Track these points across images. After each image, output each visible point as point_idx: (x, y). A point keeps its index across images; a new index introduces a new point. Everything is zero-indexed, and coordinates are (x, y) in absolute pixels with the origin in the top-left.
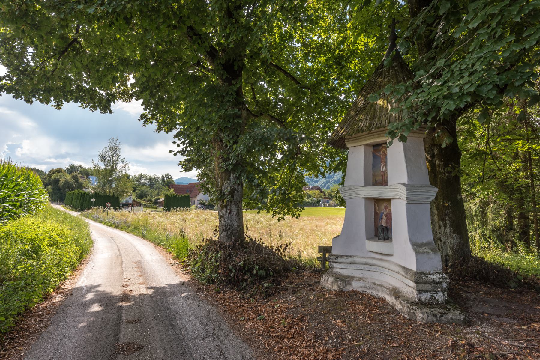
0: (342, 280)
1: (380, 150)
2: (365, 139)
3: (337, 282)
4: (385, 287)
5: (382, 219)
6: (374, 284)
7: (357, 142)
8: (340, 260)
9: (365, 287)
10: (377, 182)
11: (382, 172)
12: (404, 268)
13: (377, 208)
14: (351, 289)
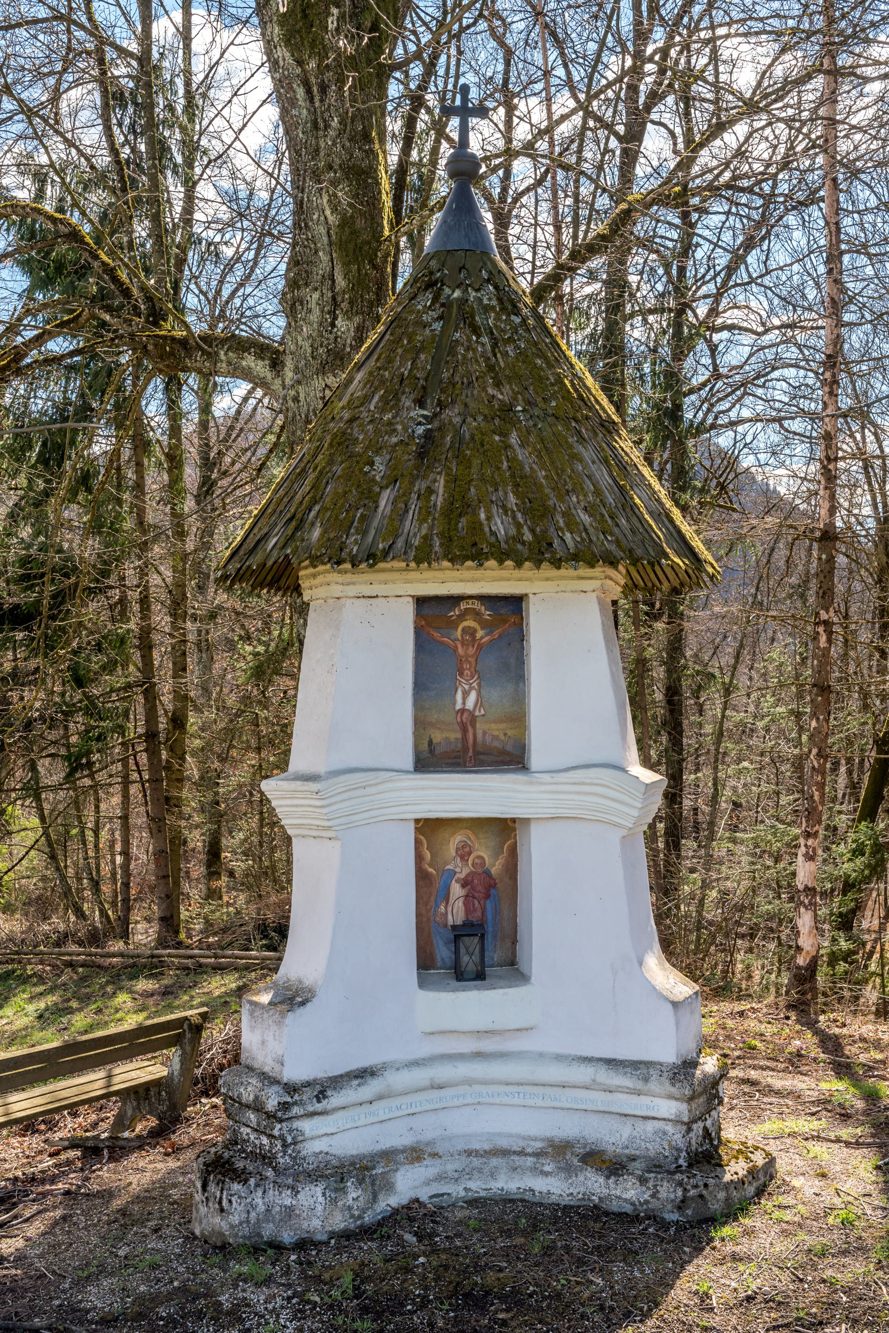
1: (452, 624)
9: (440, 1178)
11: (463, 711)
13: (428, 855)
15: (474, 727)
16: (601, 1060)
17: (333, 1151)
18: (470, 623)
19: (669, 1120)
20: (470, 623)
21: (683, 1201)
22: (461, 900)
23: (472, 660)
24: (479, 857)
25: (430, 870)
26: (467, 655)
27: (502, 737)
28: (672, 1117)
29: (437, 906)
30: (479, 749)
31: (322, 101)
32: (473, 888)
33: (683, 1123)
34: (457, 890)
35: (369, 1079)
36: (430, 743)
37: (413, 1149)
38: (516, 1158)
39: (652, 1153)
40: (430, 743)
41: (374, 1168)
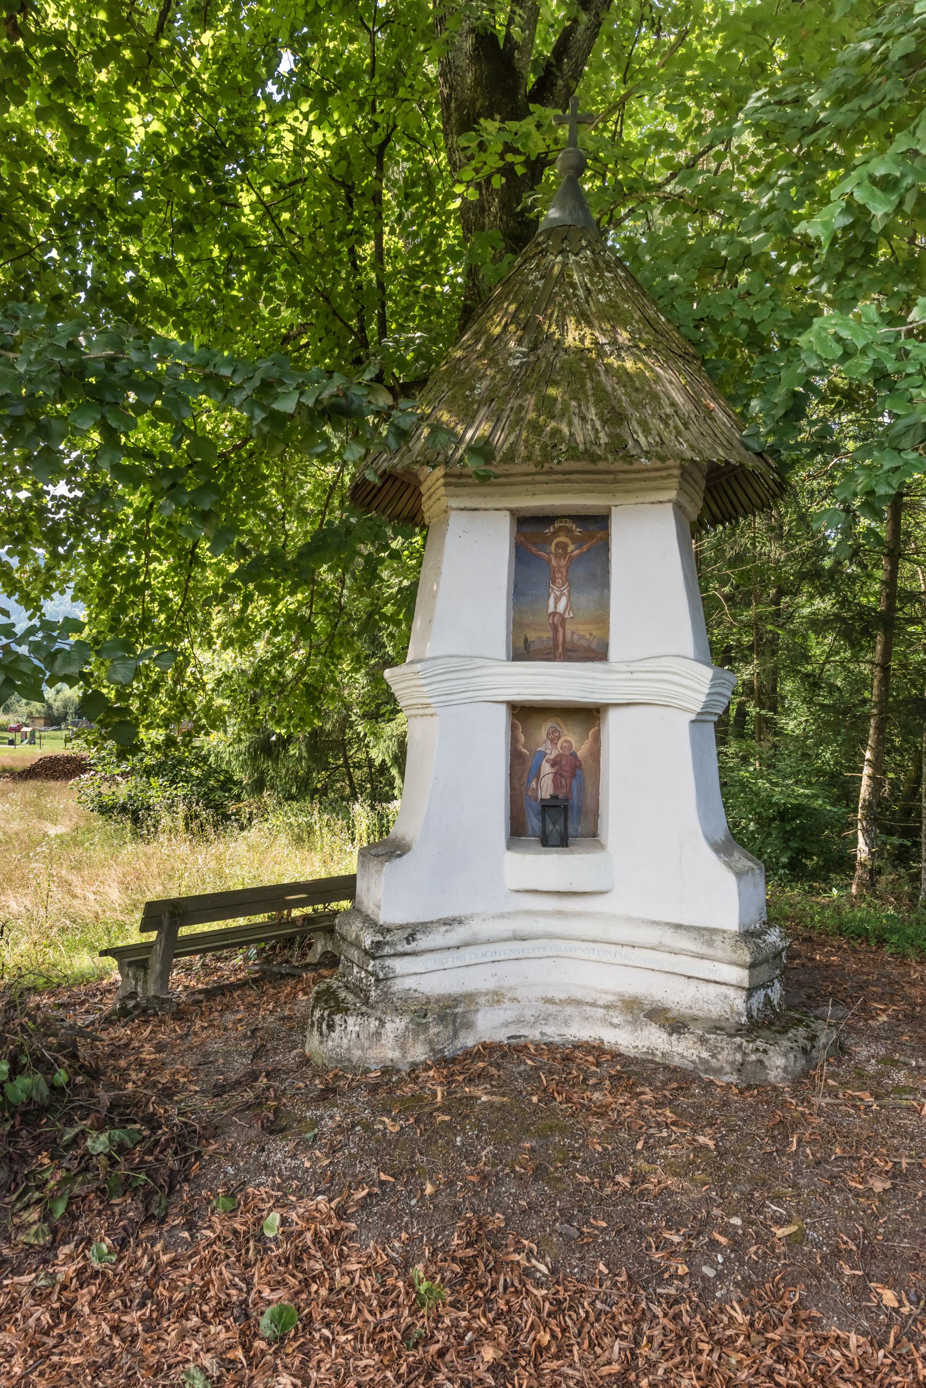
0: (441, 1018)
1: (548, 540)
2: (530, 487)
3: (426, 1027)
4: (593, 1005)
5: (538, 776)
6: (549, 1001)
7: (492, 495)
8: (423, 942)
9: (519, 1021)
10: (532, 648)
11: (554, 614)
12: (699, 930)
13: (522, 738)
14: (470, 1042)
15: (564, 629)
16: (668, 924)
17: (421, 989)
18: (562, 539)
19: (732, 985)
20: (562, 539)
21: (742, 1065)
22: (551, 776)
23: (564, 570)
24: (567, 741)
25: (524, 750)
26: (559, 567)
27: (588, 637)
28: (734, 982)
29: (529, 782)
30: (568, 646)
31: (487, 189)
32: (561, 768)
33: (743, 988)
34: (546, 768)
35: (456, 926)
36: (526, 641)
37: (496, 993)
38: (588, 1008)
39: (714, 1015)
40: (526, 641)
41: (456, 1006)
